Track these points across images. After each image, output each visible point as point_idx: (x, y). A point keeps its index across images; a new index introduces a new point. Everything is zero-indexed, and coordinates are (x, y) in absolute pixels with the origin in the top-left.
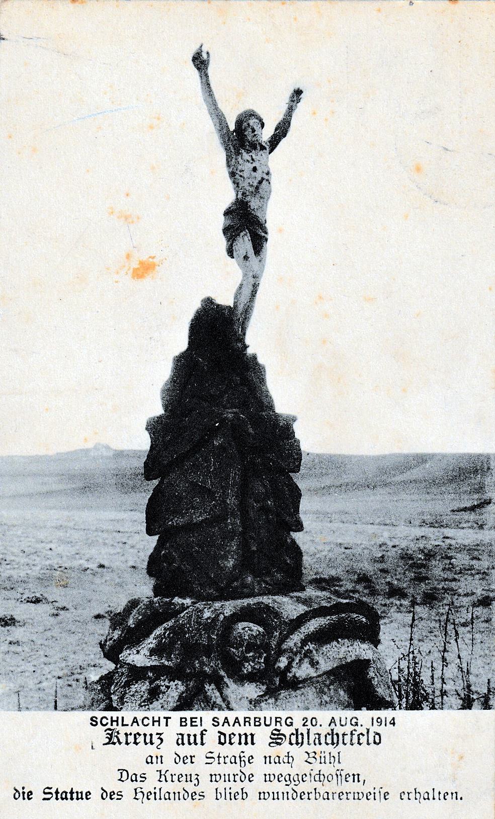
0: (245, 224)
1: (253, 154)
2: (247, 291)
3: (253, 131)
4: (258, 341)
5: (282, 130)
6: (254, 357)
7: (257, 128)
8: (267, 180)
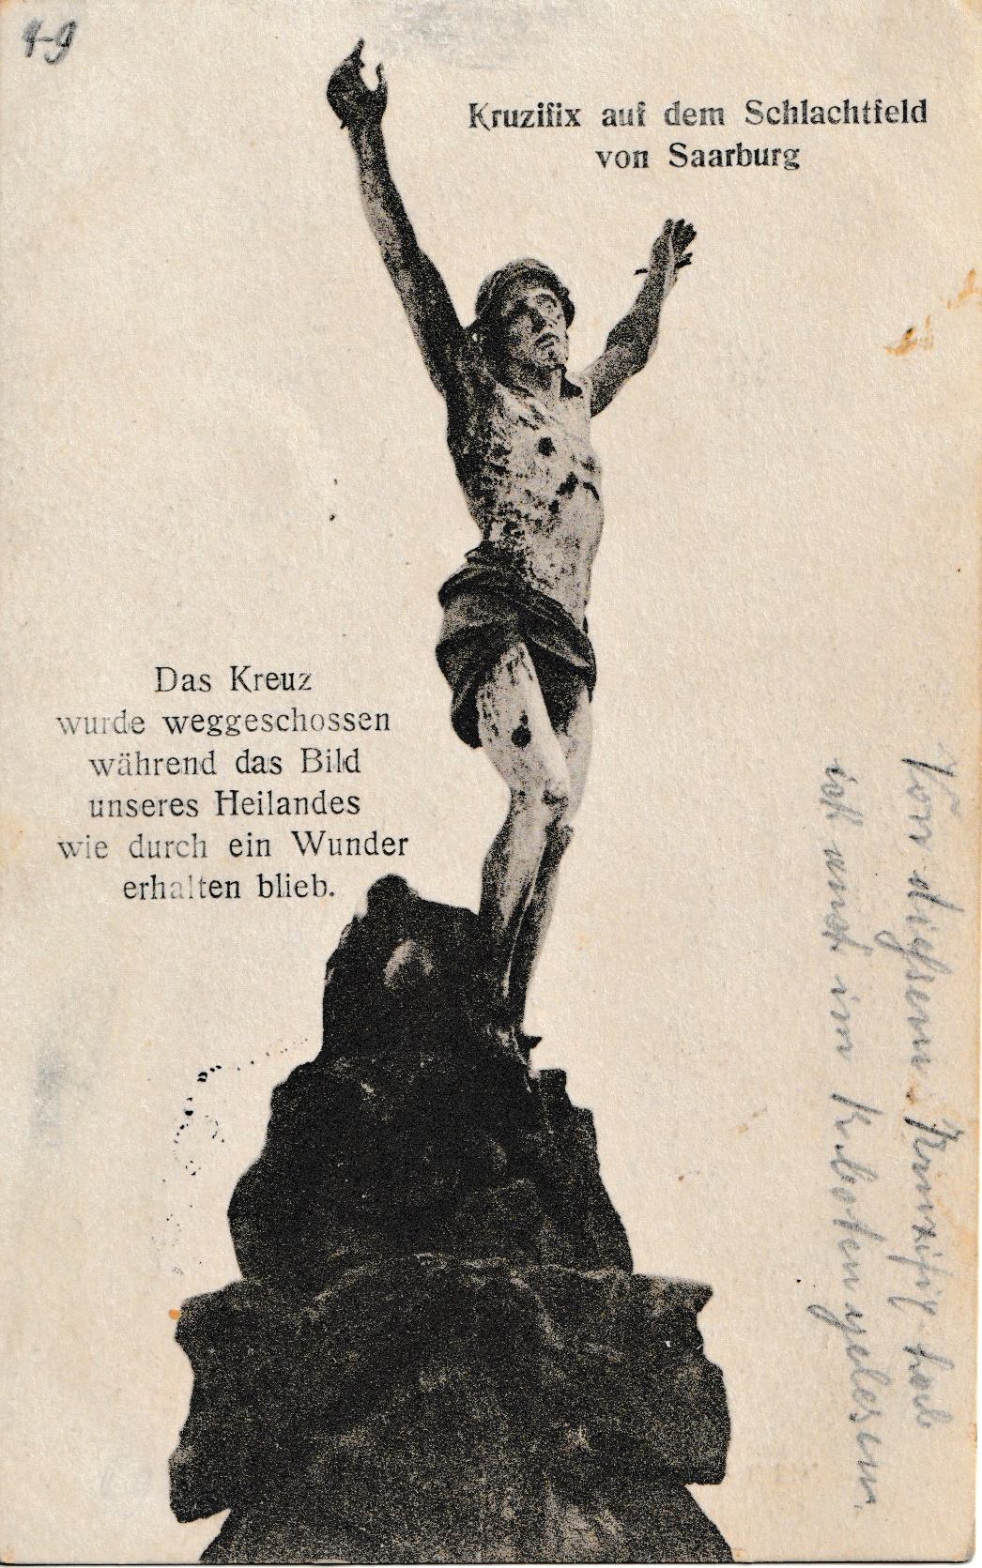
0: (510, 632)
1: (539, 400)
2: (527, 849)
3: (538, 324)
4: (568, 1020)
5: (635, 338)
6: (556, 1079)
7: (551, 313)
8: (588, 486)
